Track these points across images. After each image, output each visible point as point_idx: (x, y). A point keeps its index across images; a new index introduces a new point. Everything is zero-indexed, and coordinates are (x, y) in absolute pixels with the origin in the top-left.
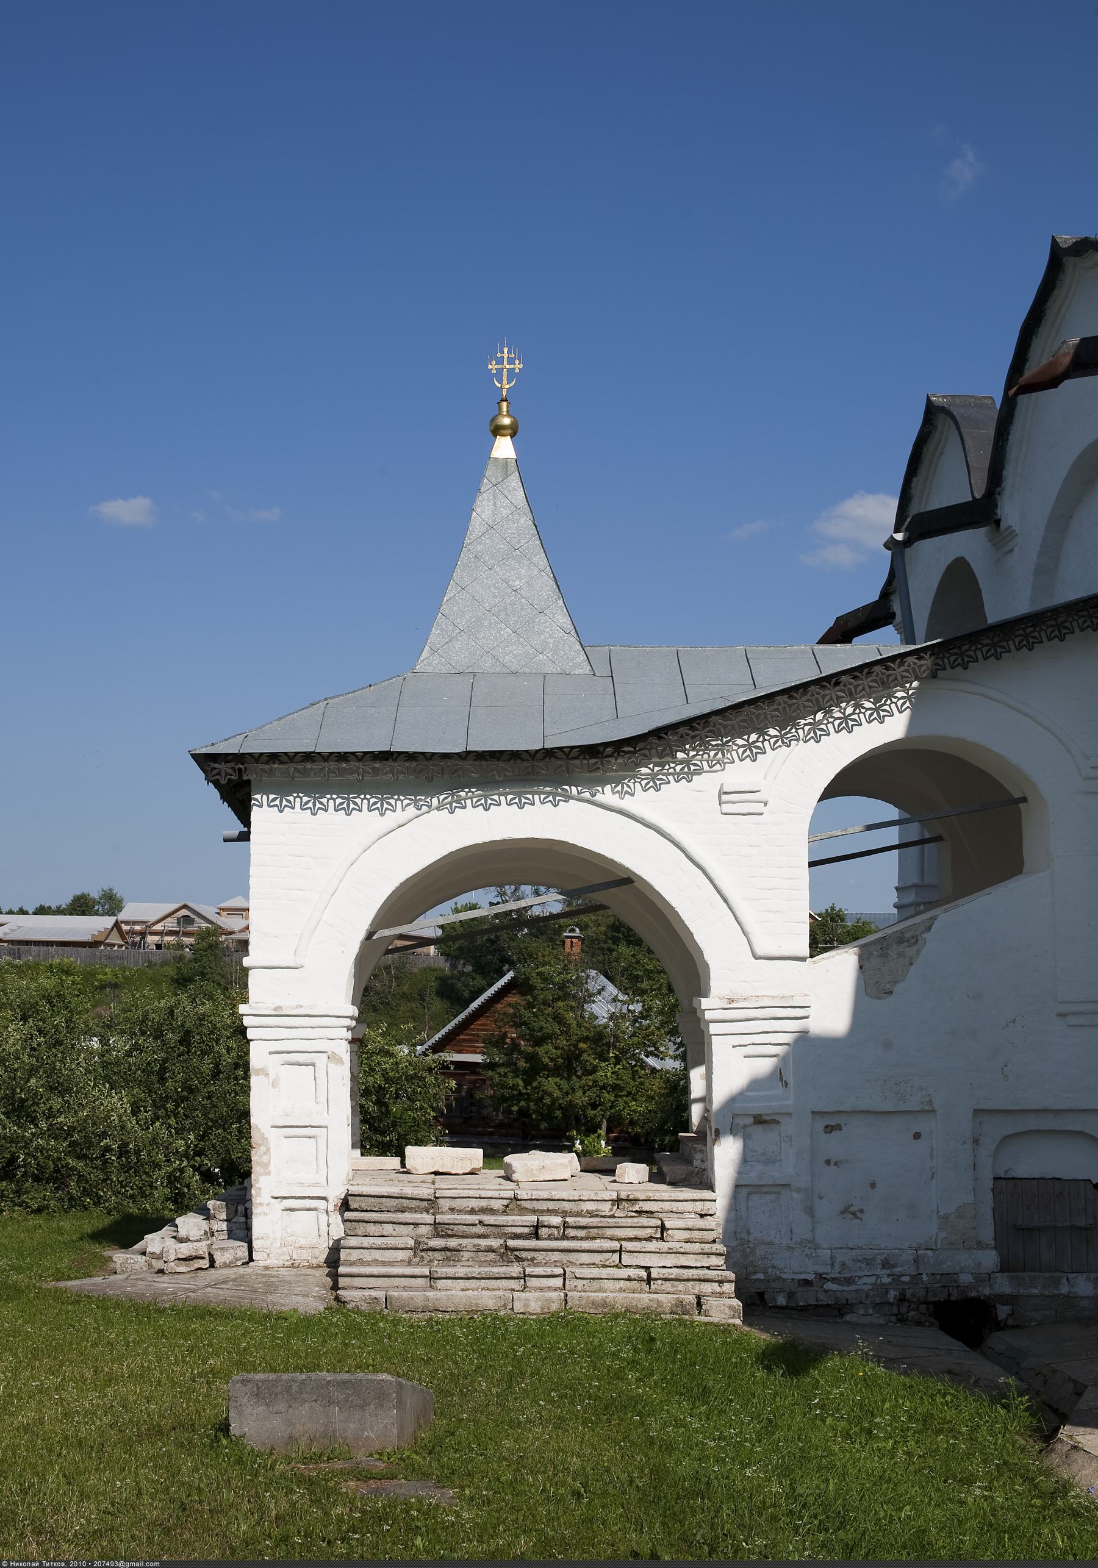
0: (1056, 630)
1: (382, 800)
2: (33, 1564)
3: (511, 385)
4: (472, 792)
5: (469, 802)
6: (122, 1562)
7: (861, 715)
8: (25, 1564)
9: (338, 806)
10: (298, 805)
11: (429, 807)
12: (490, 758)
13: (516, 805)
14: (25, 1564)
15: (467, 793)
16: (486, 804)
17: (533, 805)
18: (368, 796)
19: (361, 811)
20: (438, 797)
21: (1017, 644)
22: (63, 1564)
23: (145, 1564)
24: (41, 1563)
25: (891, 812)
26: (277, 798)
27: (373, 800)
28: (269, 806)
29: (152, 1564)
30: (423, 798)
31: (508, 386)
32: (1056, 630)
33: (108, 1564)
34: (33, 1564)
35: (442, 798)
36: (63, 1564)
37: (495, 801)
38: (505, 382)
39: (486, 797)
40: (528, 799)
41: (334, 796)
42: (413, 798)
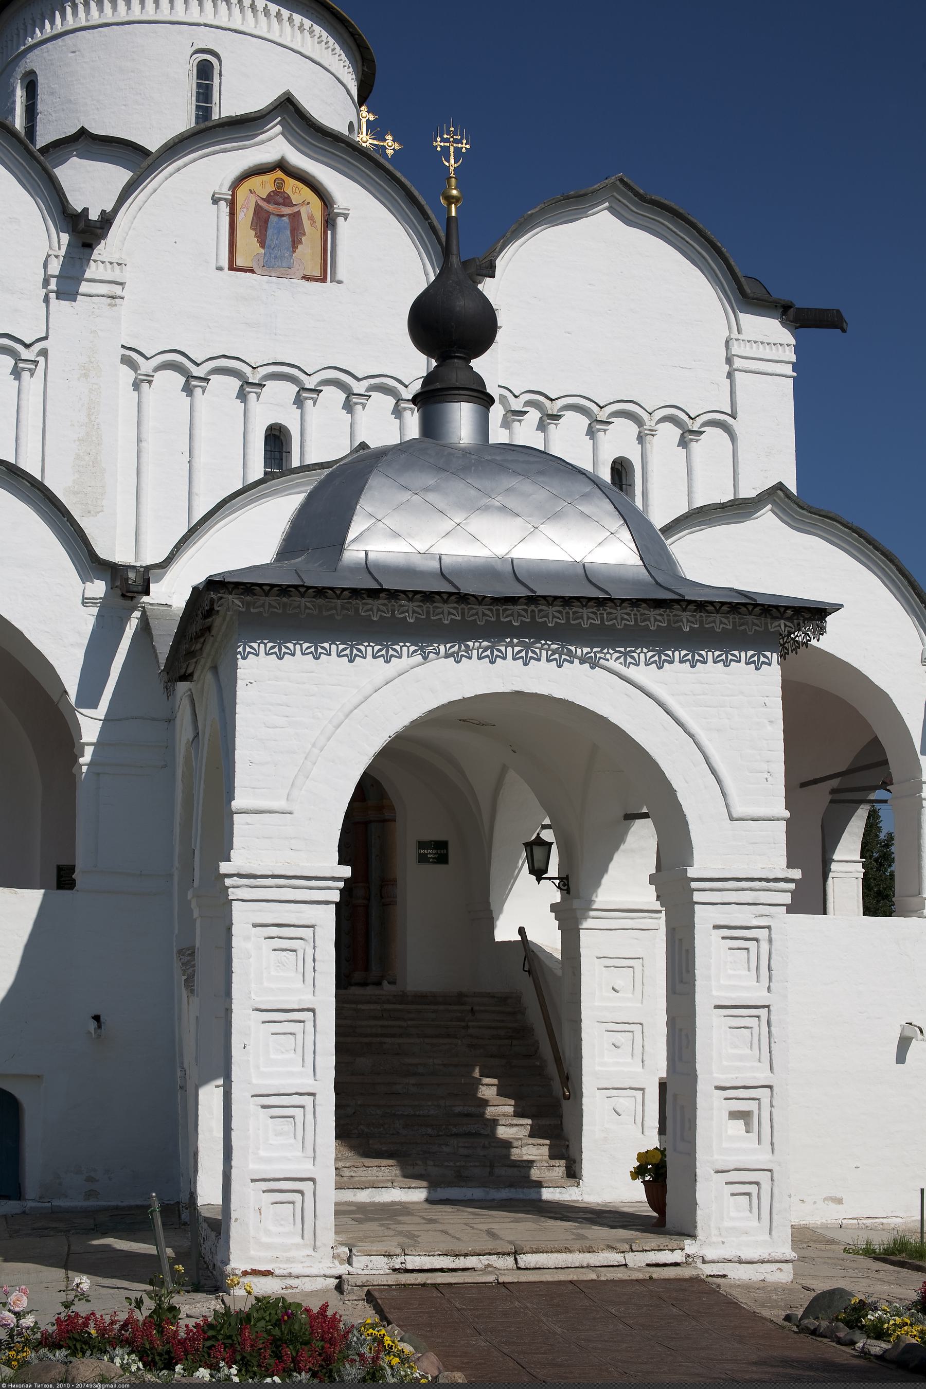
0: (242, 647)
1: (387, 647)
2: (27, 1386)
3: (459, 163)
4: (548, 644)
5: (475, 652)
6: (99, 1384)
7: (642, 655)
8: (20, 1386)
9: (377, 653)
10: (334, 653)
11: (438, 654)
12: (368, 597)
13: (274, 655)
14: (20, 1386)
15: (543, 645)
16: (351, 656)
17: (365, 658)
18: (645, 650)
19: (257, 655)
20: (713, 653)
21: (410, 653)
22: (51, 1386)
23: (117, 1386)
24: (33, 1386)
25: (78, 715)
26: (523, 650)
27: (650, 654)
28: (374, 657)
29: (123, 1386)
30: (633, 649)
31: (455, 165)
32: (242, 647)
33: (87, 1386)
34: (27, 1386)
35: (448, 646)
36: (51, 1386)
37: (254, 649)
38: (452, 161)
39: (492, 648)
40: (668, 656)
41: (408, 644)
42: (623, 650)
